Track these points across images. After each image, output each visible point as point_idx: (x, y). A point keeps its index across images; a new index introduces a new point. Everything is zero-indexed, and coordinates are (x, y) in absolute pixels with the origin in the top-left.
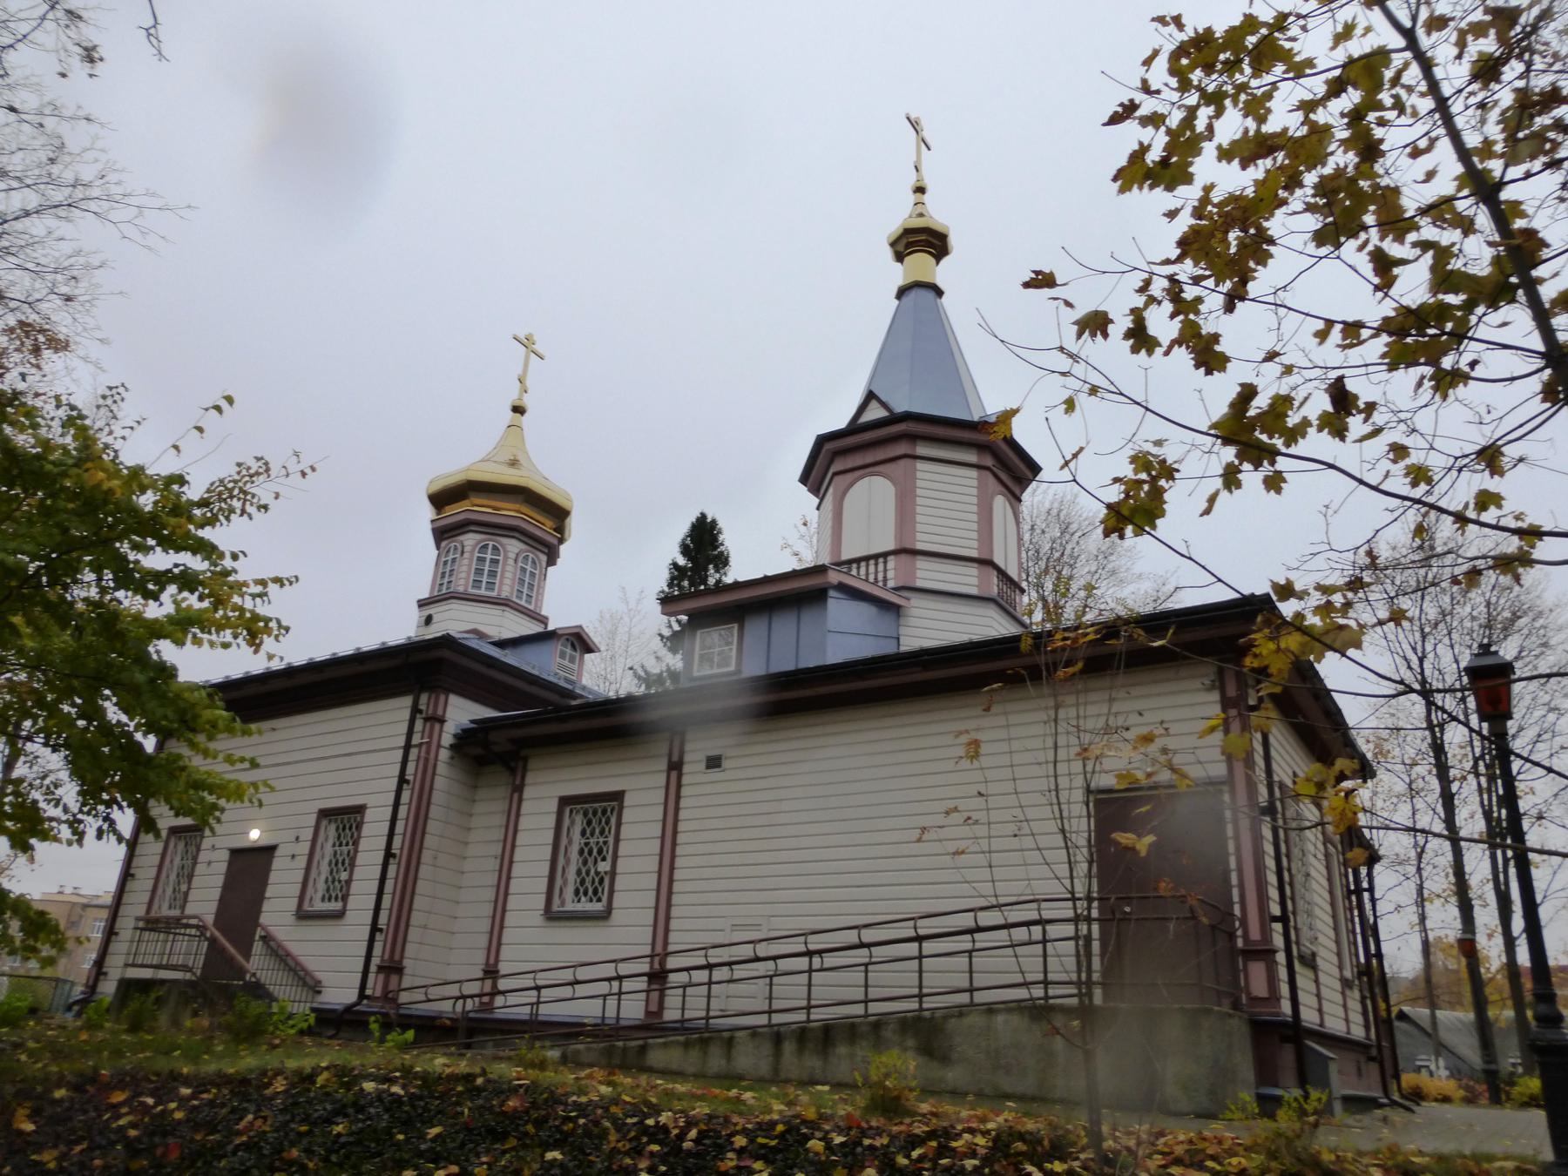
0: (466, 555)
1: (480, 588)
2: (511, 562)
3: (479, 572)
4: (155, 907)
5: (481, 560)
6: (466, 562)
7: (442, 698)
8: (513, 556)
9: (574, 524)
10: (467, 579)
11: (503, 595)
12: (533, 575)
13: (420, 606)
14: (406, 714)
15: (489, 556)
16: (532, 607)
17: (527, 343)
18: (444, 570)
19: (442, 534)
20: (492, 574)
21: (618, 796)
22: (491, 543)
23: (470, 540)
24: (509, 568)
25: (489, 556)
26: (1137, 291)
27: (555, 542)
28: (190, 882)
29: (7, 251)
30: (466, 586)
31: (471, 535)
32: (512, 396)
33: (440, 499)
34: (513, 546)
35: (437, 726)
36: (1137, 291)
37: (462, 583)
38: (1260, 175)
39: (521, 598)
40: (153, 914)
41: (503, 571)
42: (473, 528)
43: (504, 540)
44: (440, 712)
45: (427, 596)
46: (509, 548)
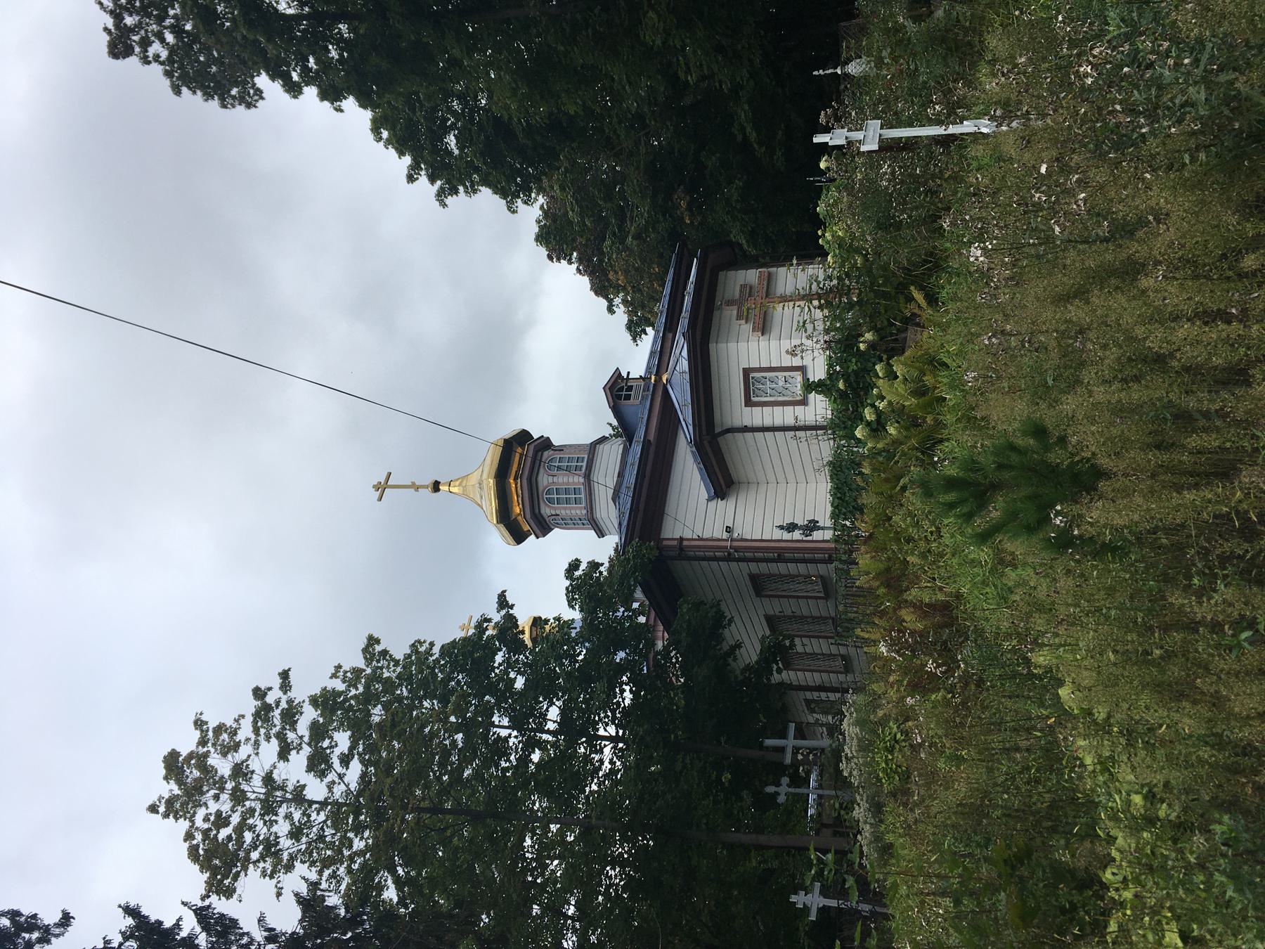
0: (558, 512)
1: (582, 466)
2: (555, 479)
3: (568, 501)
4: (838, 669)
5: (559, 468)
6: (563, 512)
7: (665, 543)
8: (550, 479)
9: (536, 615)
10: (576, 508)
11: (582, 480)
12: (561, 460)
13: (603, 536)
14: (685, 563)
15: (555, 496)
16: (586, 456)
17: (381, 488)
18: (569, 523)
19: (543, 528)
20: (567, 491)
21: (747, 372)
22: (545, 496)
23: (546, 511)
24: (560, 480)
25: (555, 496)
26: (504, 591)
27: (532, 447)
28: (806, 617)
29: (1261, 114)
30: (580, 508)
31: (542, 512)
32: (427, 493)
33: (519, 537)
34: (544, 480)
35: (685, 543)
36: (504, 591)
37: (579, 511)
38: (527, 642)
39: (582, 466)
40: (842, 670)
41: (563, 483)
42: (537, 511)
43: (541, 488)
44: (675, 543)
45: (593, 531)
46: (545, 483)
